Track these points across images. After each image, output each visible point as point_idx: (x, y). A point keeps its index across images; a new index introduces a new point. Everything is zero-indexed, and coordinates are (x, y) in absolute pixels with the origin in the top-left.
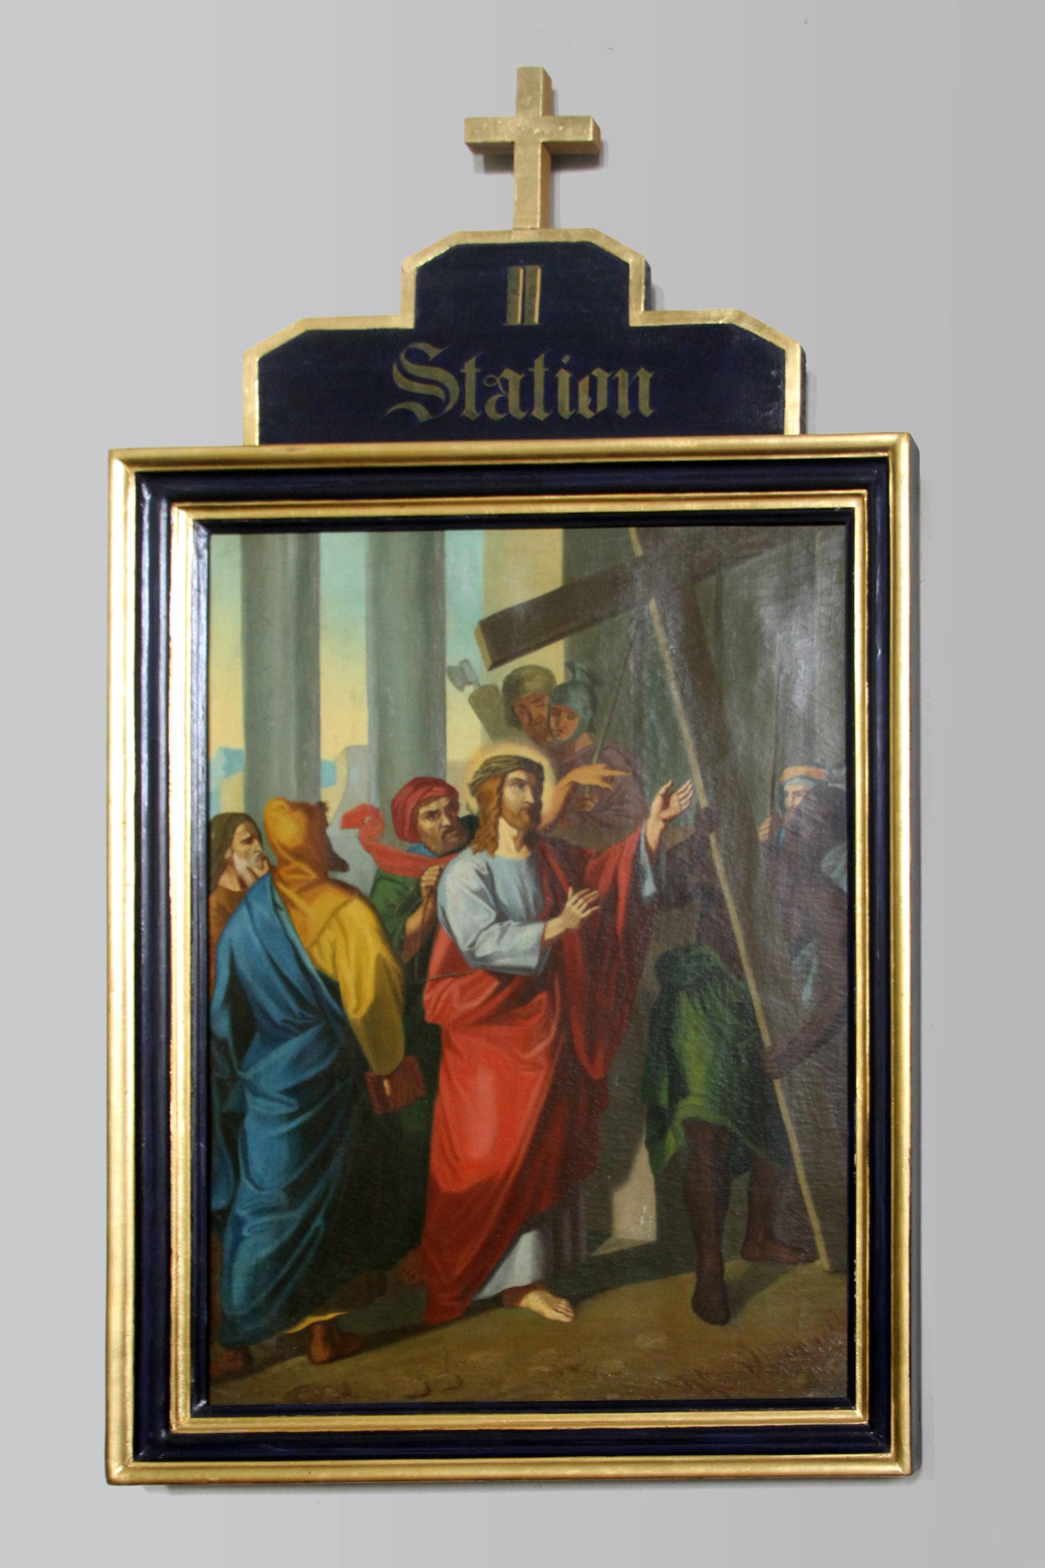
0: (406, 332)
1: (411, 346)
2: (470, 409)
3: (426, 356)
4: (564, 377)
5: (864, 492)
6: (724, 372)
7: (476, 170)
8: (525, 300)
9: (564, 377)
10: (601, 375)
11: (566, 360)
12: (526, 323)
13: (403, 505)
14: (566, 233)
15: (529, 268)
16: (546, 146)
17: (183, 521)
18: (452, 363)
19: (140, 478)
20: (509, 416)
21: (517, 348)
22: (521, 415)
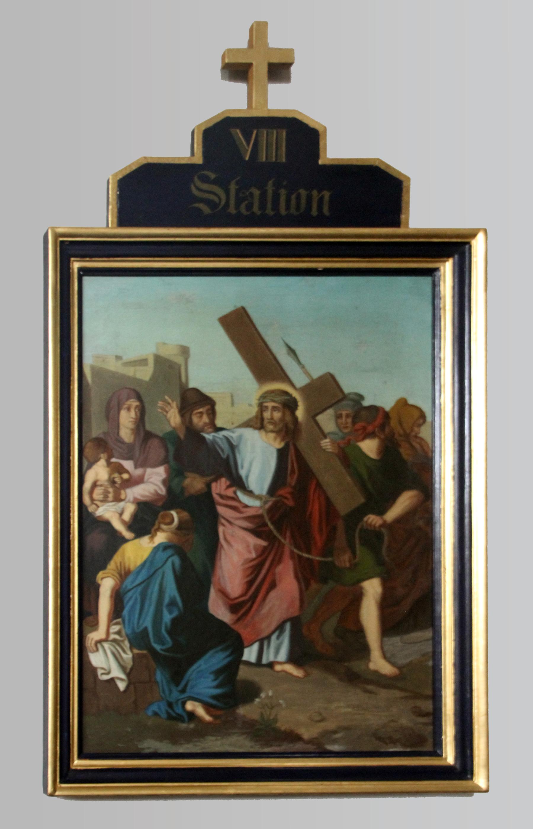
2: (232, 210)
4: (283, 192)
6: (376, 191)
9: (283, 192)
10: (303, 192)
11: (285, 183)
12: (278, 161)
13: (375, 262)
15: (270, 130)
22: (259, 213)
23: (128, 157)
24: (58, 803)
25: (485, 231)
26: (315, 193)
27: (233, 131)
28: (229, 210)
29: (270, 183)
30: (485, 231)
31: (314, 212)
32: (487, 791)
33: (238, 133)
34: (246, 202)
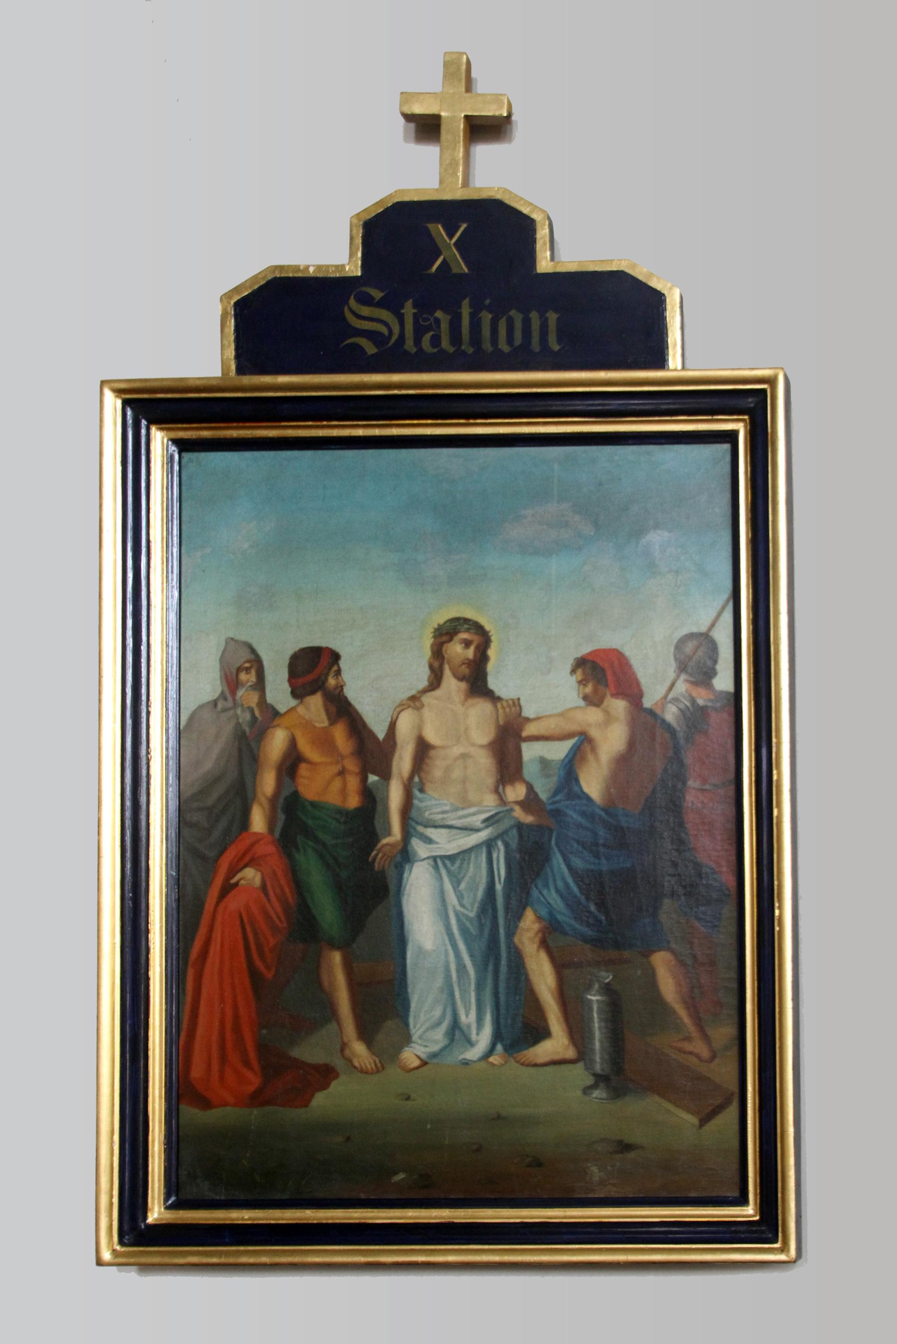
0: (356, 278)
1: (364, 289)
3: (373, 298)
4: (486, 317)
5: (746, 417)
6: (618, 316)
7: (406, 139)
8: (449, 248)
9: (486, 317)
11: (488, 302)
14: (480, 189)
16: (466, 117)
17: (159, 441)
18: (392, 304)
19: (126, 403)
20: (442, 351)
21: (441, 292)
22: (451, 350)
23: (248, 264)
24: (131, 1280)
25: (99, 1263)
26: (534, 316)
27: (431, 226)
28: (406, 347)
29: (466, 303)
30: (99, 1263)
31: (536, 346)
32: (103, 383)
33: (438, 230)
34: (431, 333)
